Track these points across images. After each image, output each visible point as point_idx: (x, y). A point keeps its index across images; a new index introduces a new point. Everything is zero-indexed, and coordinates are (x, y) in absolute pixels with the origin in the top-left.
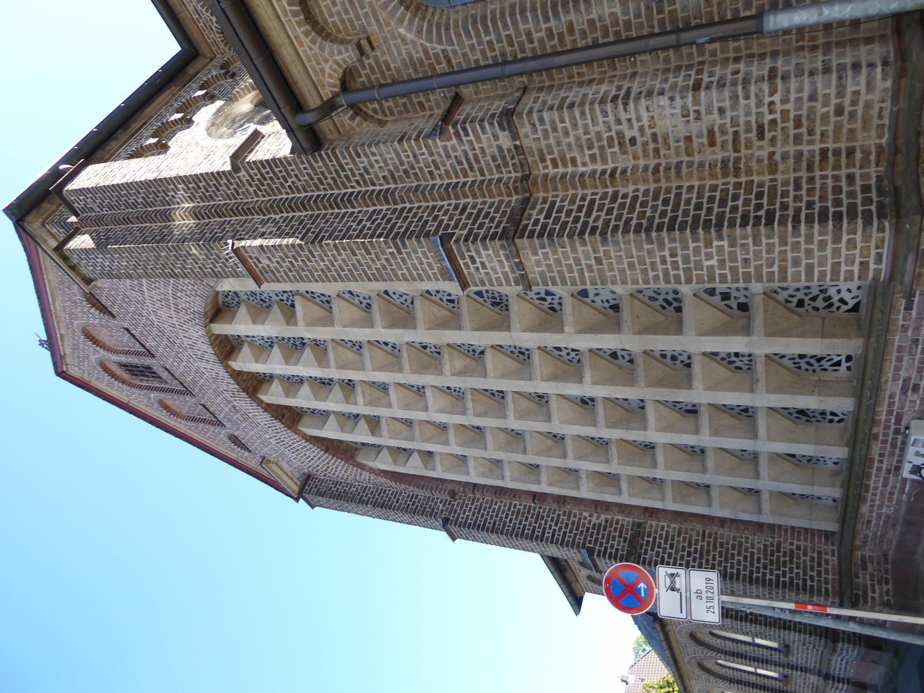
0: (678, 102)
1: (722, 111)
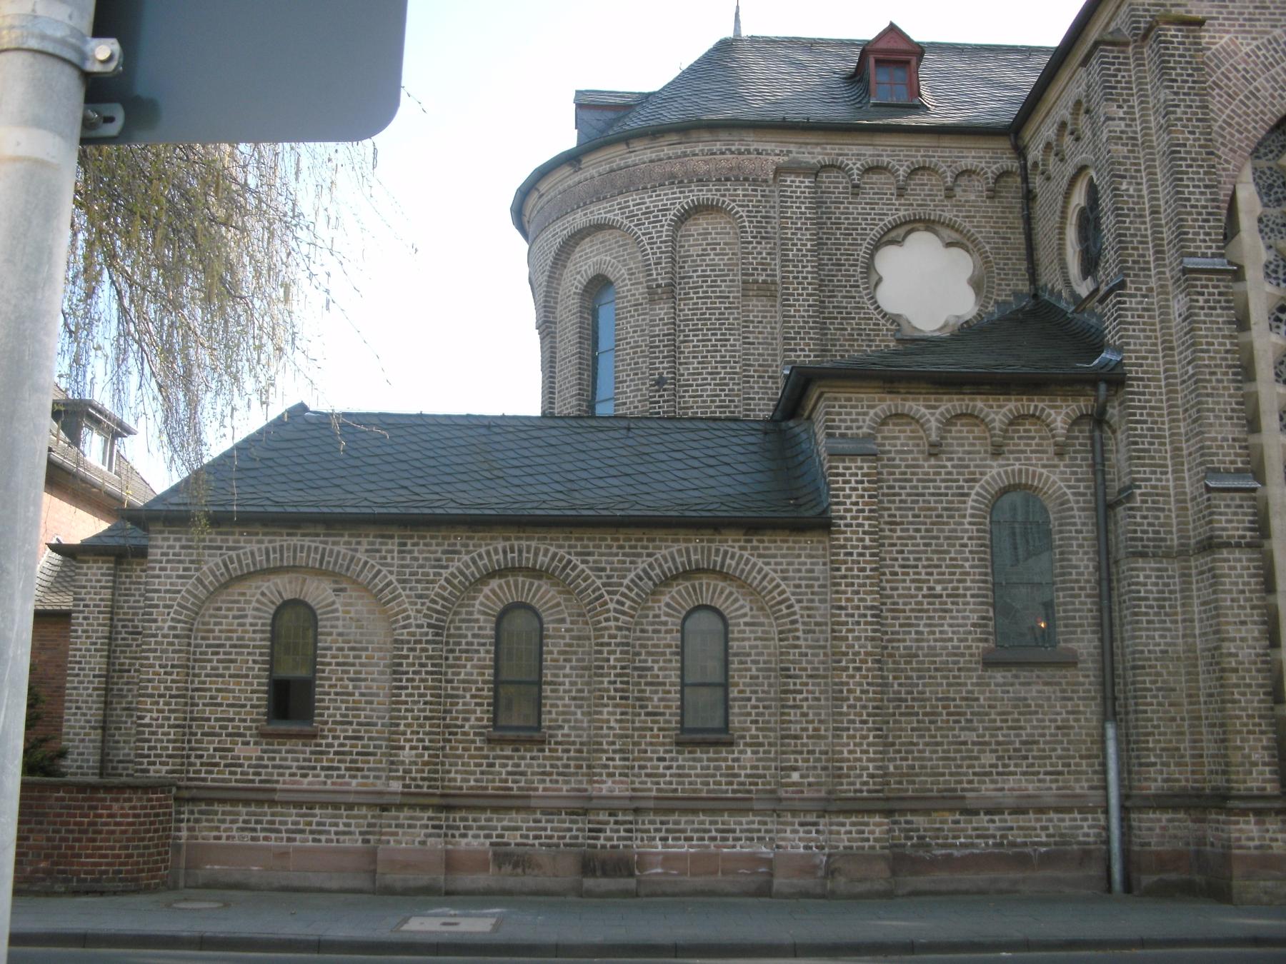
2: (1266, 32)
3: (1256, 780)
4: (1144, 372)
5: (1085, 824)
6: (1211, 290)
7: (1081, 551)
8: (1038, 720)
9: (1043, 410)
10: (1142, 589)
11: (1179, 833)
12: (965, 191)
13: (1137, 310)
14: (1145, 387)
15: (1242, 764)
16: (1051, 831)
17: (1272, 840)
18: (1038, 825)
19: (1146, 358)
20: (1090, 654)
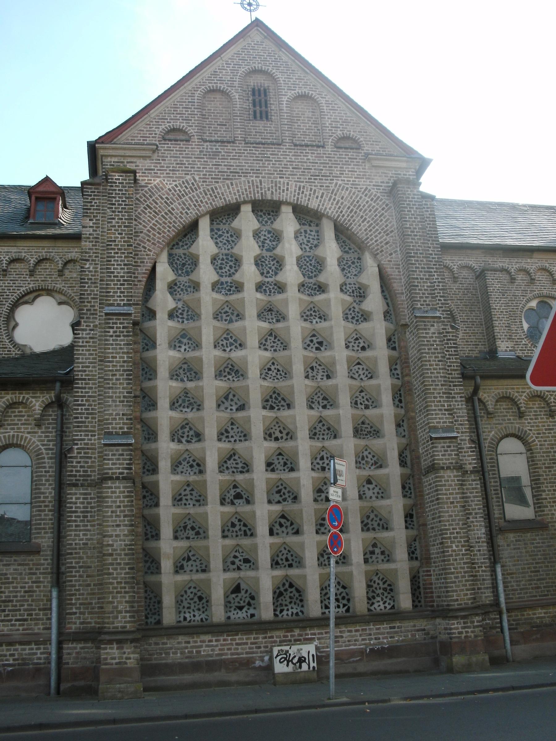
0: (483, 536)
1: (479, 551)
2: (182, 178)
3: (121, 622)
4: (86, 375)
5: (39, 652)
6: (119, 325)
7: (47, 483)
8: (13, 587)
9: (28, 399)
10: (74, 506)
11: (88, 656)
12: (70, 272)
13: (86, 338)
14: (86, 384)
15: (112, 612)
16: (16, 657)
17: (127, 658)
18: (8, 653)
19: (89, 367)
20: (48, 546)
